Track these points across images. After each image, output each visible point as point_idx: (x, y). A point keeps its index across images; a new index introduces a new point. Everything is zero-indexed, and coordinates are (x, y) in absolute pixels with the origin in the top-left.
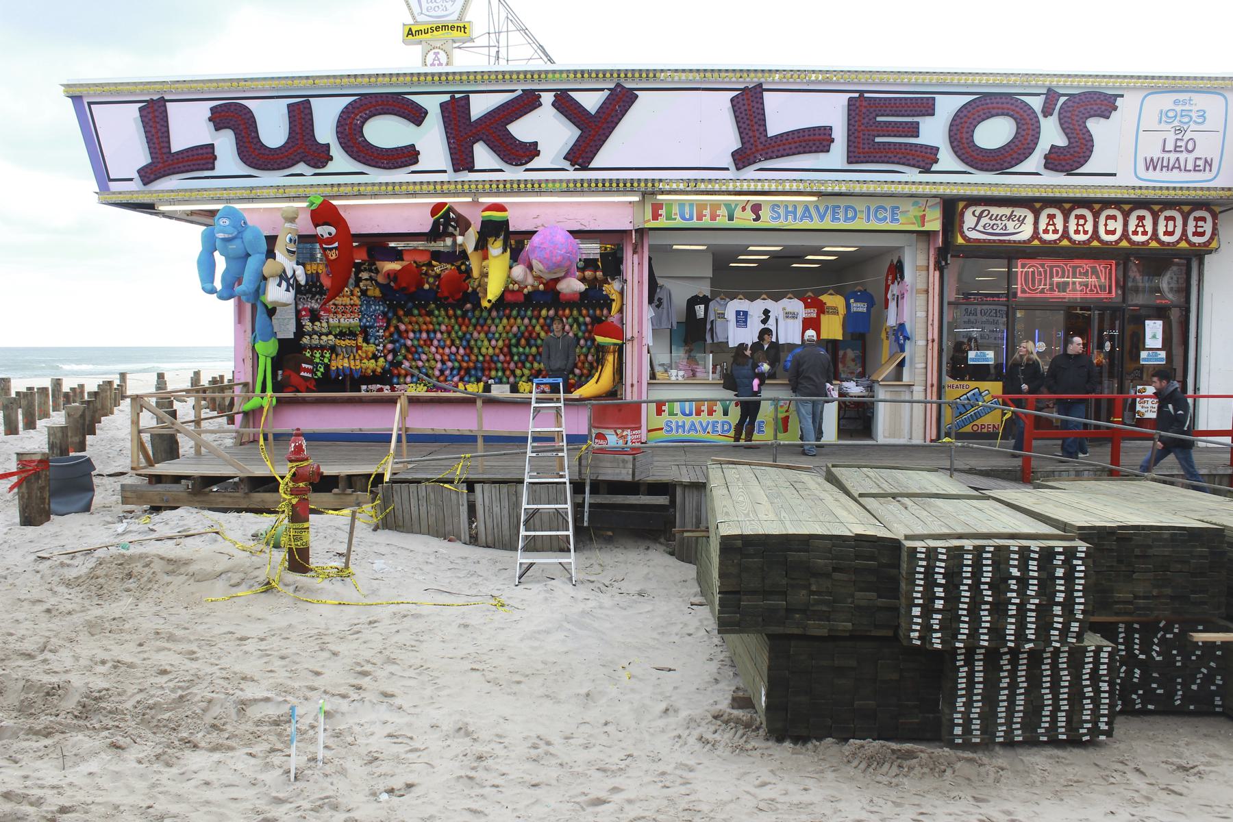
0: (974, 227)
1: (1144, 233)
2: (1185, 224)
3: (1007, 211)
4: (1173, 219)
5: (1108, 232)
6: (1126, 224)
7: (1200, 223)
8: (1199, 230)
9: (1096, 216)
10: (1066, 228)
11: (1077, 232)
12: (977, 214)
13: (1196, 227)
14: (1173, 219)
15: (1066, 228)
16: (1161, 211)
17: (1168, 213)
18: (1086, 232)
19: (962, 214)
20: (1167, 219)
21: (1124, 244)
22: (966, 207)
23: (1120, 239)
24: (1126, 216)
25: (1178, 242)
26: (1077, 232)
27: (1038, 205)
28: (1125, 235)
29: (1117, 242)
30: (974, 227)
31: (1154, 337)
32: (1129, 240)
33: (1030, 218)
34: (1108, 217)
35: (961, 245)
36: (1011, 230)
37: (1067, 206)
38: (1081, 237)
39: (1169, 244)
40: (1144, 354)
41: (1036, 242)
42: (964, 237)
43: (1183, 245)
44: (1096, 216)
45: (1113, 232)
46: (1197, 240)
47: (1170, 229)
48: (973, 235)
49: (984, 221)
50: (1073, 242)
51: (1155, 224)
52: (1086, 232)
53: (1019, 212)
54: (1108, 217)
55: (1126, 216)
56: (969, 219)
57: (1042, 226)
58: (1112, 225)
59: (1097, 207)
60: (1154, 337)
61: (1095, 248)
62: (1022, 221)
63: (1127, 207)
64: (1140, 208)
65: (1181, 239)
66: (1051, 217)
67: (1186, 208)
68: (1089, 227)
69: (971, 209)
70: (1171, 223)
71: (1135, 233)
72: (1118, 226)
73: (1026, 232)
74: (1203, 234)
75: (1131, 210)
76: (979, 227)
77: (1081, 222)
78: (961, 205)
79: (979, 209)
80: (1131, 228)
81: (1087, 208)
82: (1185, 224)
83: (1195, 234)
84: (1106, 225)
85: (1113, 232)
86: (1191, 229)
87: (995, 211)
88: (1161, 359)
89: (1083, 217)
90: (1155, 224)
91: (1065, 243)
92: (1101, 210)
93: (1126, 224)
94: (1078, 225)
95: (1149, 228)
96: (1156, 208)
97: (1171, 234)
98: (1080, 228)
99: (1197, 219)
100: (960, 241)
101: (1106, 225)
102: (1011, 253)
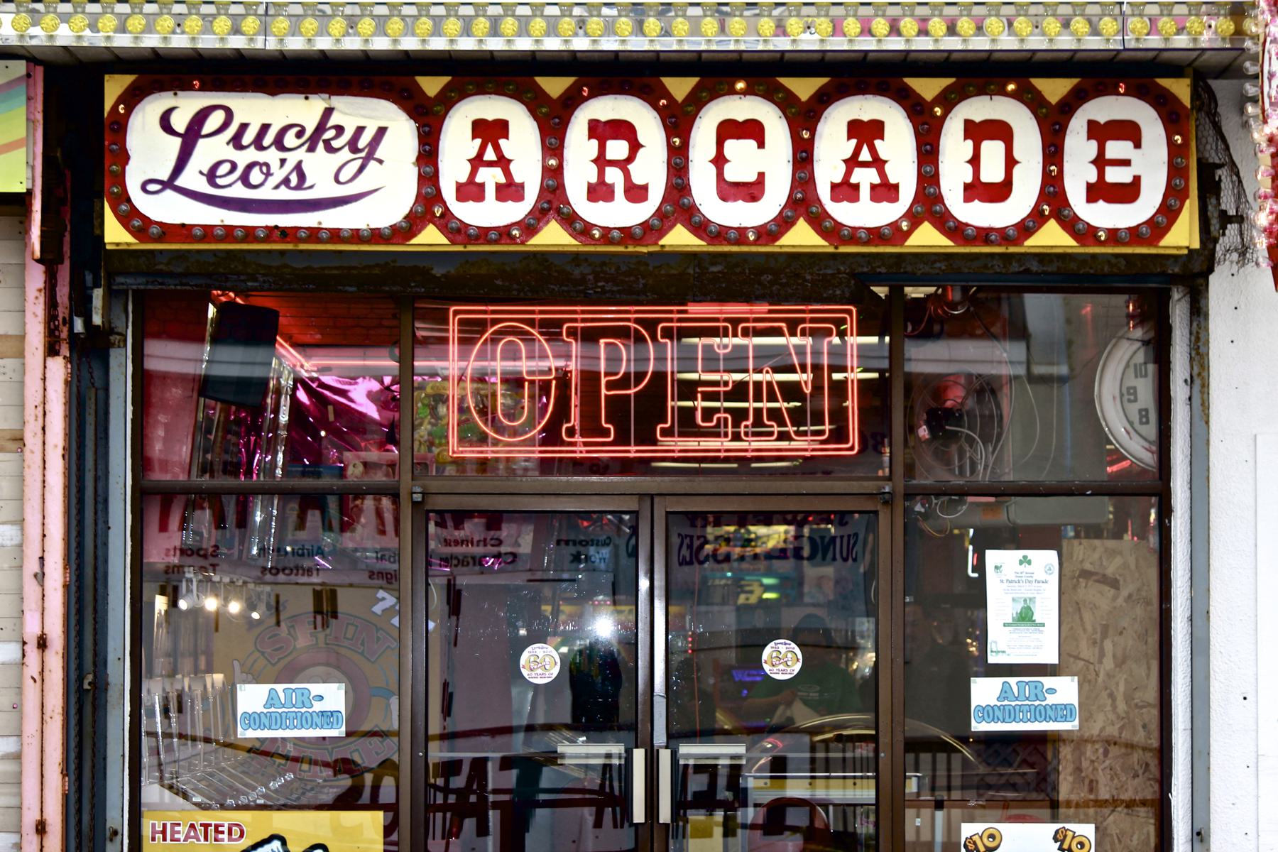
0: (166, 175)
1: (885, 191)
2: (1053, 153)
3: (302, 110)
4: (1001, 131)
5: (730, 191)
6: (803, 157)
7: (1115, 149)
8: (1115, 175)
9: (678, 123)
10: (553, 177)
11: (599, 192)
12: (180, 122)
13: (1101, 162)
14: (1001, 131)
15: (553, 177)
16: (949, 100)
17: (979, 108)
18: (636, 193)
19: (120, 126)
20: (977, 132)
21: (802, 237)
22: (132, 98)
23: (783, 223)
24: (804, 120)
25: (1026, 228)
26: (599, 192)
27: (432, 85)
28: (803, 202)
29: (768, 233)
30: (166, 175)
31: (1025, 617)
32: (820, 221)
33: (402, 133)
34: (729, 130)
35: (123, 254)
36: (322, 187)
37: (555, 86)
38: (620, 214)
39: (984, 235)
40: (984, 691)
41: (431, 237)
42: (130, 216)
43: (1052, 237)
44: (678, 123)
45: (753, 191)
46: (1104, 216)
47: (992, 172)
48: (166, 209)
49: (209, 151)
50: (1084, 233)
51: (928, 152)
52: (636, 193)
53: (356, 113)
54: (729, 130)
55: (804, 120)
56: (147, 146)
57: (453, 169)
58: (744, 160)
59: (680, 87)
60: (1025, 617)
61: (546, 258)
62: (367, 150)
63: (804, 88)
64: (481, 91)
65: (914, 218)
66: (491, 131)
67: (1054, 89)
68: (651, 167)
69: (152, 108)
70: (993, 151)
71: (844, 190)
72: (771, 160)
73: (384, 198)
74: (1128, 193)
75: (823, 100)
76: (192, 178)
77: (618, 149)
78: (114, 87)
79: (186, 106)
80: (828, 170)
81: (517, 96)
82: (1053, 153)
83: (1097, 192)
84: (720, 161)
85: (753, 191)
86: (1078, 173)
87: (253, 109)
88: (1062, 711)
89: (623, 129)
90: (928, 152)
91: (553, 236)
92: (697, 102)
93: (803, 157)
94: (601, 162)
95: (903, 171)
96: (928, 88)
97: (1000, 192)
98: (614, 176)
99: (1099, 132)
100: (115, 233)
101: (720, 161)
102: (378, 290)
